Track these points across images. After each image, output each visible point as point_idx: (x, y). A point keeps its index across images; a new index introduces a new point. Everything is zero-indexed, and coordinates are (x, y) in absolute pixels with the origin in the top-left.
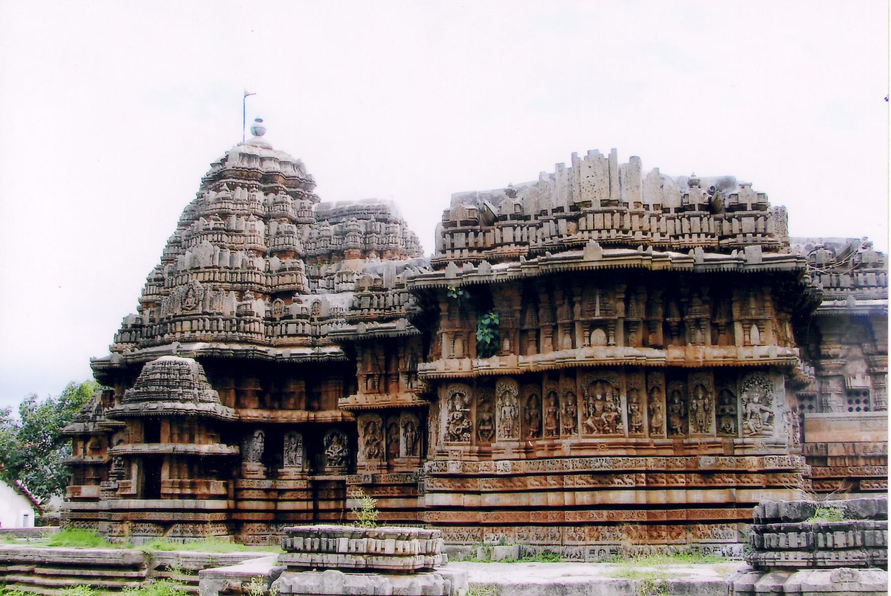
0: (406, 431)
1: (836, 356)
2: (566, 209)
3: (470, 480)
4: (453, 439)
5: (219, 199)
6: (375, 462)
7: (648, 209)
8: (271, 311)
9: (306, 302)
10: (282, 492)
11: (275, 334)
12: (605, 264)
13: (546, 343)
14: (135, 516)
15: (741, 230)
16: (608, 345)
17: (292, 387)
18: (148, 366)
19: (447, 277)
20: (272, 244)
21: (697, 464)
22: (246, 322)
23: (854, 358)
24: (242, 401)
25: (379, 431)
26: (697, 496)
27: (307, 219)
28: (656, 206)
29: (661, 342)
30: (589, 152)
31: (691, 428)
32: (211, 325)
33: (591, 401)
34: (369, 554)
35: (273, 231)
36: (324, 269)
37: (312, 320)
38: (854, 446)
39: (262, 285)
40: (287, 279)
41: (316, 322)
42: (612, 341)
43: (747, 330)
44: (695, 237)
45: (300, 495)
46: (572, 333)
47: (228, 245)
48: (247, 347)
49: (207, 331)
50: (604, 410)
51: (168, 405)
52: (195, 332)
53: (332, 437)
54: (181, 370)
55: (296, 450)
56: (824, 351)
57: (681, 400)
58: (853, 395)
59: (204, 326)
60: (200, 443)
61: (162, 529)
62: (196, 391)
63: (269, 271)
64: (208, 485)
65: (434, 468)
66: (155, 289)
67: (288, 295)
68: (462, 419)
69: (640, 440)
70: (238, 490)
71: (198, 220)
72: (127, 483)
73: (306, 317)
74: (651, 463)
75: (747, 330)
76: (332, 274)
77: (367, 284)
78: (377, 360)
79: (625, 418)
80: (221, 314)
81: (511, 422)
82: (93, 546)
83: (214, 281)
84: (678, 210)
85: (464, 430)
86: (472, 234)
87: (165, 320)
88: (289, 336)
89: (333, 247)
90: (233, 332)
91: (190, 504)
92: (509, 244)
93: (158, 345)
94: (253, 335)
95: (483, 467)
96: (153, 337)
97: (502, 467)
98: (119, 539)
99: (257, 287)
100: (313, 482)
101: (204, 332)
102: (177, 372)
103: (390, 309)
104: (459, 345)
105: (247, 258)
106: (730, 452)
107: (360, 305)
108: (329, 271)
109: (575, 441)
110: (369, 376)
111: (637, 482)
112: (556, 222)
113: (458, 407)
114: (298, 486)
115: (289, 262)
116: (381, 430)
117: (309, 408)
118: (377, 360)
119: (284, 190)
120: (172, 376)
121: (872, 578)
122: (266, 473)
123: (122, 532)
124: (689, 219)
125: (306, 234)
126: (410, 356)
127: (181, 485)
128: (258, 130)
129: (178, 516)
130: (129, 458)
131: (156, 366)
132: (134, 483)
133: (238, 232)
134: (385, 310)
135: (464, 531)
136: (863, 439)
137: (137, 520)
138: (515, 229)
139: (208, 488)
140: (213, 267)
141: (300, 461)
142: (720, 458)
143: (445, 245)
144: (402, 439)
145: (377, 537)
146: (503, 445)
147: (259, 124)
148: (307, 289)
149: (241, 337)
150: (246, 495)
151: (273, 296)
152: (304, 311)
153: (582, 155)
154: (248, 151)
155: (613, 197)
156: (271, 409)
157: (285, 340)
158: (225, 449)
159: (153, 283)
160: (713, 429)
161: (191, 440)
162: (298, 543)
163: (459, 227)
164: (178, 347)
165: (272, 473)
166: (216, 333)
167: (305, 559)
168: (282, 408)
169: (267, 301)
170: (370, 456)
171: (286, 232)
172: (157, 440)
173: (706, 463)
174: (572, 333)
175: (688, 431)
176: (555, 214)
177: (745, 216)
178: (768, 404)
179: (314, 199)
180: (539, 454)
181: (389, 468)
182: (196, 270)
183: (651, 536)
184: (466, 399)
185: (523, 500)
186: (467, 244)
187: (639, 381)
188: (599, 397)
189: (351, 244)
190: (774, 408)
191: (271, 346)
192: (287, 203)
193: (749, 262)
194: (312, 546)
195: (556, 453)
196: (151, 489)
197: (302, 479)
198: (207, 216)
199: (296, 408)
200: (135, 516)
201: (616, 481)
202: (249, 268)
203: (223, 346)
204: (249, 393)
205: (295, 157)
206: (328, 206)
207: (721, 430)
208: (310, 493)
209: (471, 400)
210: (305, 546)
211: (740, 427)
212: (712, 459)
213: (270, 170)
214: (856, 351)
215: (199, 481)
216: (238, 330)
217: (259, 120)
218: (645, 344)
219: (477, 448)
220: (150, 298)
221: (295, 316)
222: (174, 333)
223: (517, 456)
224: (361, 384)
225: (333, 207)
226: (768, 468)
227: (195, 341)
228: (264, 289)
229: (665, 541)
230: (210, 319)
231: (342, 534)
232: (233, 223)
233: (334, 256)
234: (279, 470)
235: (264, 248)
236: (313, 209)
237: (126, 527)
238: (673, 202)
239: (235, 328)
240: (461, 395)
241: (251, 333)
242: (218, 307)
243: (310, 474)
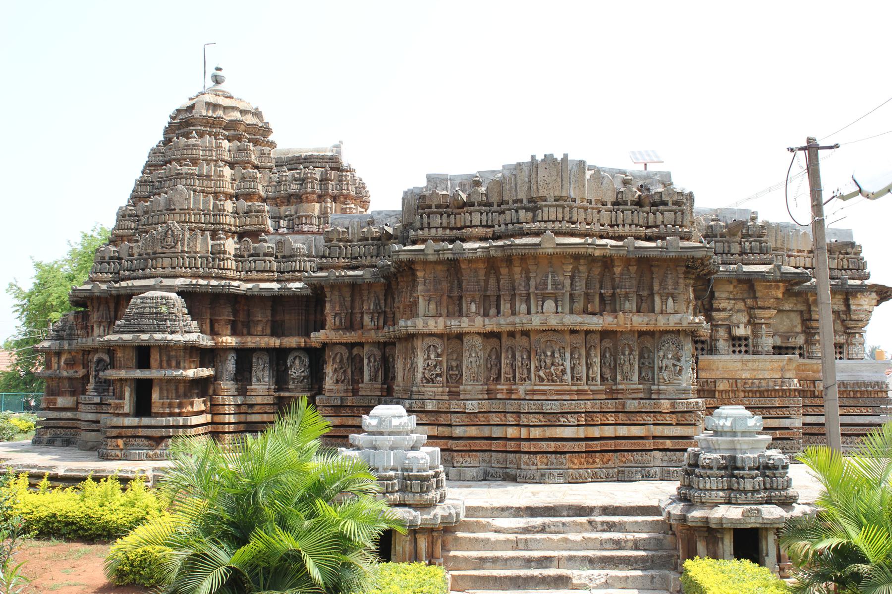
0: (369, 362)
1: (724, 310)
2: (525, 201)
4: (428, 382)
6: (342, 387)
7: (590, 203)
8: (239, 249)
10: (251, 406)
12: (558, 250)
13: (505, 307)
14: (129, 432)
15: (663, 222)
16: (557, 313)
21: (624, 405)
22: (220, 260)
23: (738, 311)
26: (623, 431)
28: (597, 201)
29: (597, 310)
30: (545, 156)
31: (619, 377)
33: (543, 357)
38: (736, 382)
40: (255, 220)
42: (560, 309)
43: (664, 302)
44: (627, 226)
45: (267, 409)
46: (528, 301)
48: (223, 282)
50: (553, 364)
53: (295, 359)
55: (263, 370)
56: (715, 305)
57: (611, 355)
58: (736, 341)
61: (154, 443)
64: (192, 404)
65: (414, 405)
67: (255, 235)
68: (435, 366)
69: (580, 388)
72: (120, 404)
73: (272, 255)
74: (589, 406)
75: (664, 302)
77: (335, 237)
79: (569, 371)
81: (476, 370)
84: (614, 204)
86: (445, 216)
88: (257, 271)
92: (476, 226)
95: (454, 406)
97: (471, 406)
98: (113, 452)
99: (227, 227)
100: (280, 398)
103: (356, 258)
104: (432, 306)
106: (648, 396)
109: (529, 388)
110: (336, 314)
111: (578, 421)
112: (517, 211)
113: (432, 356)
114: (265, 402)
117: (274, 334)
118: (344, 300)
119: (246, 138)
121: (772, 513)
122: (237, 390)
124: (622, 212)
126: (373, 299)
127: (170, 406)
132: (127, 405)
134: (352, 259)
136: (743, 376)
138: (481, 214)
139: (192, 407)
141: (267, 379)
142: (642, 401)
144: (366, 369)
146: (469, 387)
147: (219, 73)
148: (272, 230)
153: (540, 157)
154: (212, 101)
155: (564, 194)
160: (635, 378)
161: (178, 367)
168: (249, 334)
169: (236, 239)
173: (632, 405)
174: (528, 301)
175: (616, 379)
176: (516, 205)
177: (666, 211)
178: (679, 360)
179: (272, 145)
180: (499, 396)
181: (355, 392)
183: (588, 462)
184: (439, 351)
185: (486, 432)
187: (579, 339)
188: (549, 354)
190: (683, 363)
193: (670, 250)
195: (513, 397)
199: (263, 335)
201: (562, 420)
202: (220, 211)
203: (202, 282)
205: (252, 105)
207: (641, 379)
208: (276, 407)
209: (443, 351)
211: (656, 377)
212: (636, 402)
214: (741, 305)
218: (585, 311)
219: (447, 389)
223: (481, 397)
226: (678, 410)
228: (233, 229)
229: (599, 466)
233: (293, 199)
237: (120, 442)
238: (610, 198)
243: (276, 391)
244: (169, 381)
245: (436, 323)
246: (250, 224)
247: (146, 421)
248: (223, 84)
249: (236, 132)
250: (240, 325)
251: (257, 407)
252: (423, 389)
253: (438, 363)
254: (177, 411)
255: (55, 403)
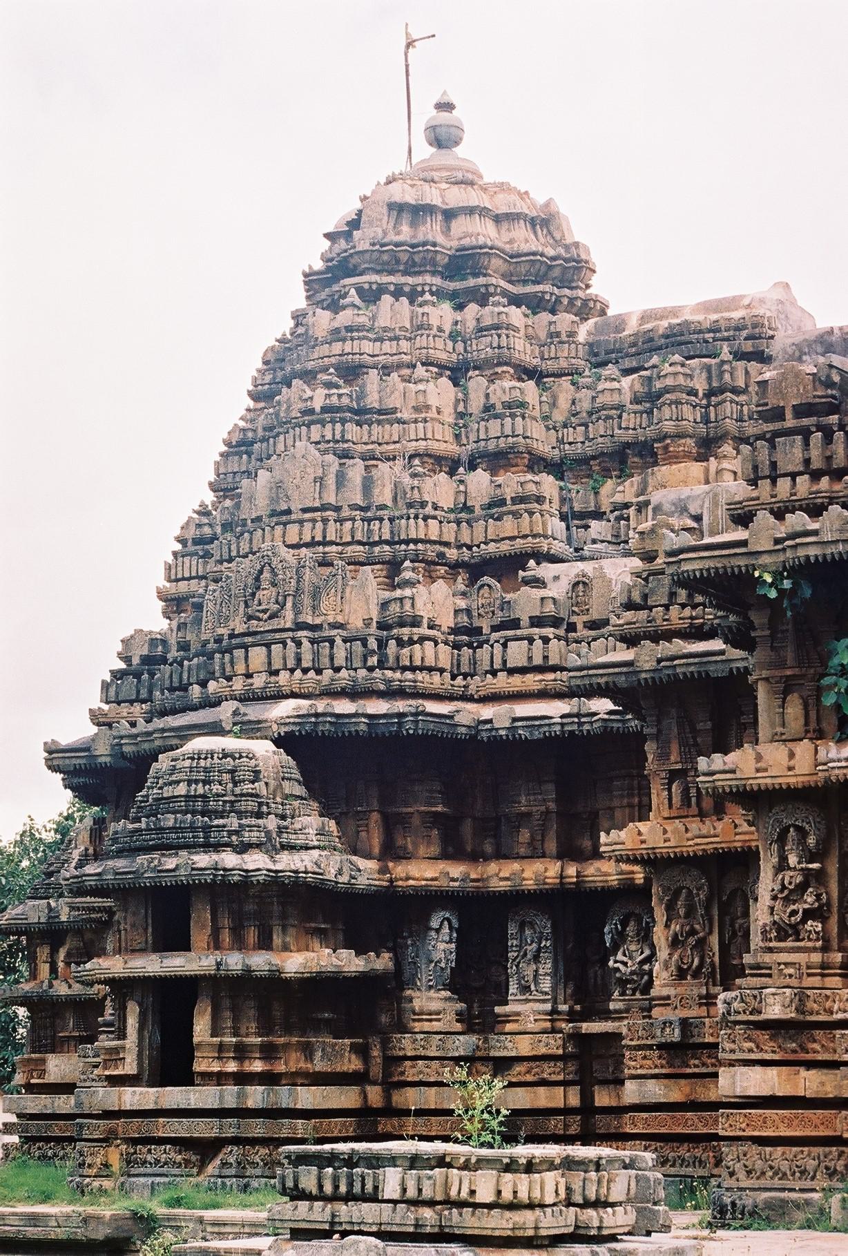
3: (818, 1034)
5: (336, 331)
6: (693, 988)
8: (468, 611)
9: (558, 580)
11: (480, 669)
14: (135, 1128)
17: (523, 800)
18: (163, 762)
19: (752, 547)
20: (473, 437)
22: (401, 643)
24: (400, 842)
25: (701, 911)
27: (563, 364)
32: (316, 655)
34: (449, 1203)
35: (476, 404)
36: (614, 492)
37: (572, 627)
39: (447, 544)
41: (582, 632)
47: (361, 448)
48: (401, 706)
49: (305, 671)
51: (203, 860)
52: (276, 673)
53: (625, 924)
54: (236, 770)
55: (536, 958)
59: (299, 660)
60: (286, 948)
62: (271, 823)
63: (466, 508)
64: (308, 1051)
66: (192, 566)
67: (507, 567)
68: (802, 888)
70: (392, 1061)
71: (289, 386)
73: (555, 622)
76: (627, 506)
78: (694, 730)
80: (341, 626)
82: (43, 1202)
83: (325, 543)
85: (809, 914)
87: (212, 646)
88: (512, 672)
89: (628, 436)
90: (371, 669)
91: (256, 1096)
93: (194, 708)
94: (419, 676)
96: (184, 688)
98: (96, 1184)
99: (431, 552)
100: (576, 1037)
101: (298, 673)
102: (226, 777)
104: (794, 709)
105: (407, 480)
107: (645, 597)
108: (618, 498)
113: (793, 860)
114: (543, 1051)
115: (512, 482)
116: (708, 908)
117: (568, 853)
118: (694, 730)
119: (505, 293)
120: (216, 788)
122: (460, 1016)
123: (106, 1165)
125: (564, 403)
127: (241, 1052)
128: (442, 132)
129: (230, 1128)
130: (123, 987)
131: (179, 764)
133: (386, 414)
135: (808, 1158)
137: (137, 1136)
139: (310, 1057)
140: (324, 508)
141: (546, 984)
143: (755, 468)
145: (466, 1167)
147: (444, 116)
149: (388, 682)
150: (411, 1072)
151: (477, 570)
152: (550, 608)
154: (410, 198)
156: (475, 857)
157: (502, 682)
158: (349, 962)
159: (191, 548)
161: (265, 944)
162: (308, 1179)
163: (790, 422)
164: (236, 713)
165: (481, 1015)
166: (328, 673)
167: (318, 1213)
168: (501, 854)
170: (681, 974)
171: (508, 405)
172: (182, 944)
179: (585, 309)
182: (282, 516)
186: (807, 462)
189: (668, 427)
191: (470, 699)
192: (509, 327)
194: (336, 1187)
196: (171, 1064)
197: (554, 1031)
198: (309, 376)
199: (536, 853)
200: (135, 1128)
203: (344, 706)
204: (416, 821)
206: (619, 324)
210: (321, 1187)
213: (466, 242)
215: (282, 1040)
216: (382, 665)
217: (445, 106)
220: (183, 586)
221: (525, 621)
222: (229, 679)
224: (658, 796)
225: (632, 327)
227: (280, 696)
230: (313, 641)
231: (392, 1160)
232: (373, 389)
234: (497, 1009)
235: (452, 448)
236: (582, 337)
237: (114, 1156)
239: (373, 661)
240: (799, 829)
241: (413, 669)
242: (329, 611)
243: (572, 1017)
244: (245, 983)
245: (792, 755)
246: (497, 537)
247: (174, 1096)
248: (459, 151)
249: (481, 280)
250: (467, 828)
251: (519, 1068)
252: (768, 958)
253: (812, 879)
254: (258, 1066)
255: (43, 1073)
